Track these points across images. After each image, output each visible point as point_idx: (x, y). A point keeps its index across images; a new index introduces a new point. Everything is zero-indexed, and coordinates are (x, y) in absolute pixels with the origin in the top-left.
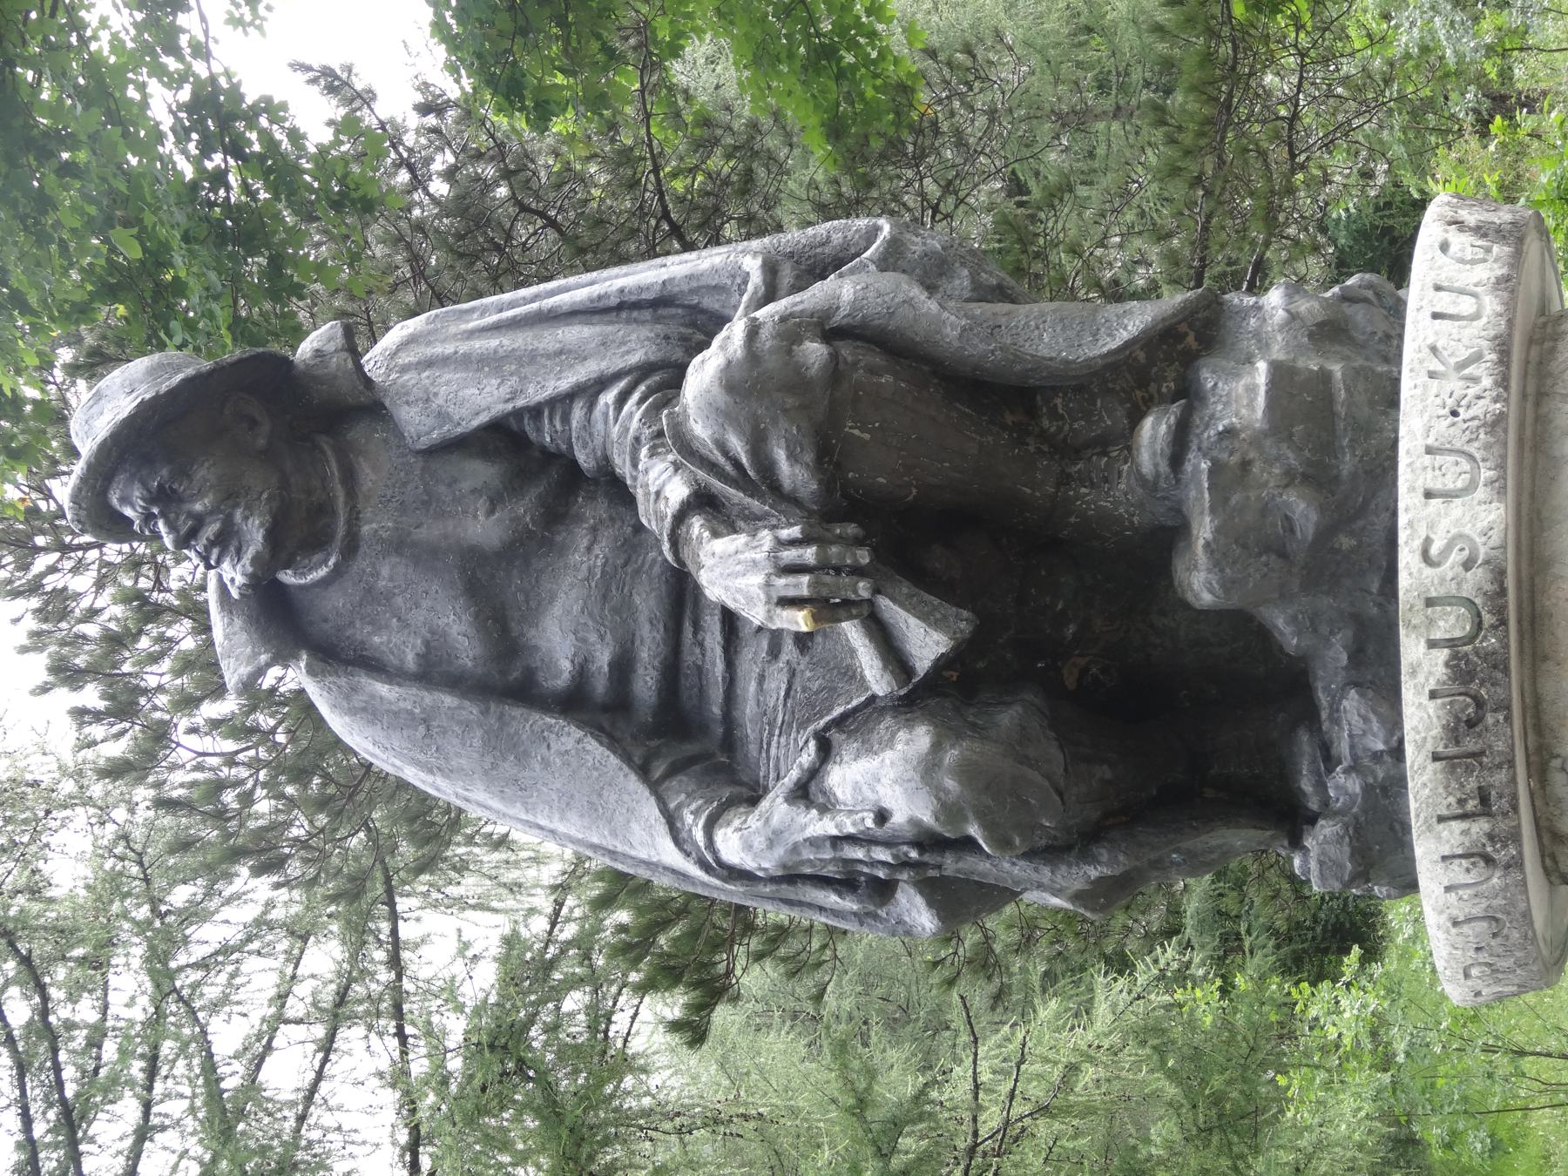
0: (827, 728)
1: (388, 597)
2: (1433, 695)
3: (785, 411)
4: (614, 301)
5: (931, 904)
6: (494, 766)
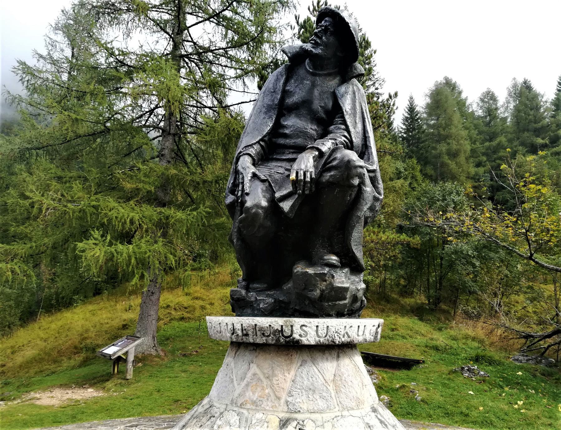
0: (269, 182)
1: (302, 83)
2: (270, 326)
3: (342, 175)
4: (367, 135)
5: (231, 202)
6: (264, 107)
